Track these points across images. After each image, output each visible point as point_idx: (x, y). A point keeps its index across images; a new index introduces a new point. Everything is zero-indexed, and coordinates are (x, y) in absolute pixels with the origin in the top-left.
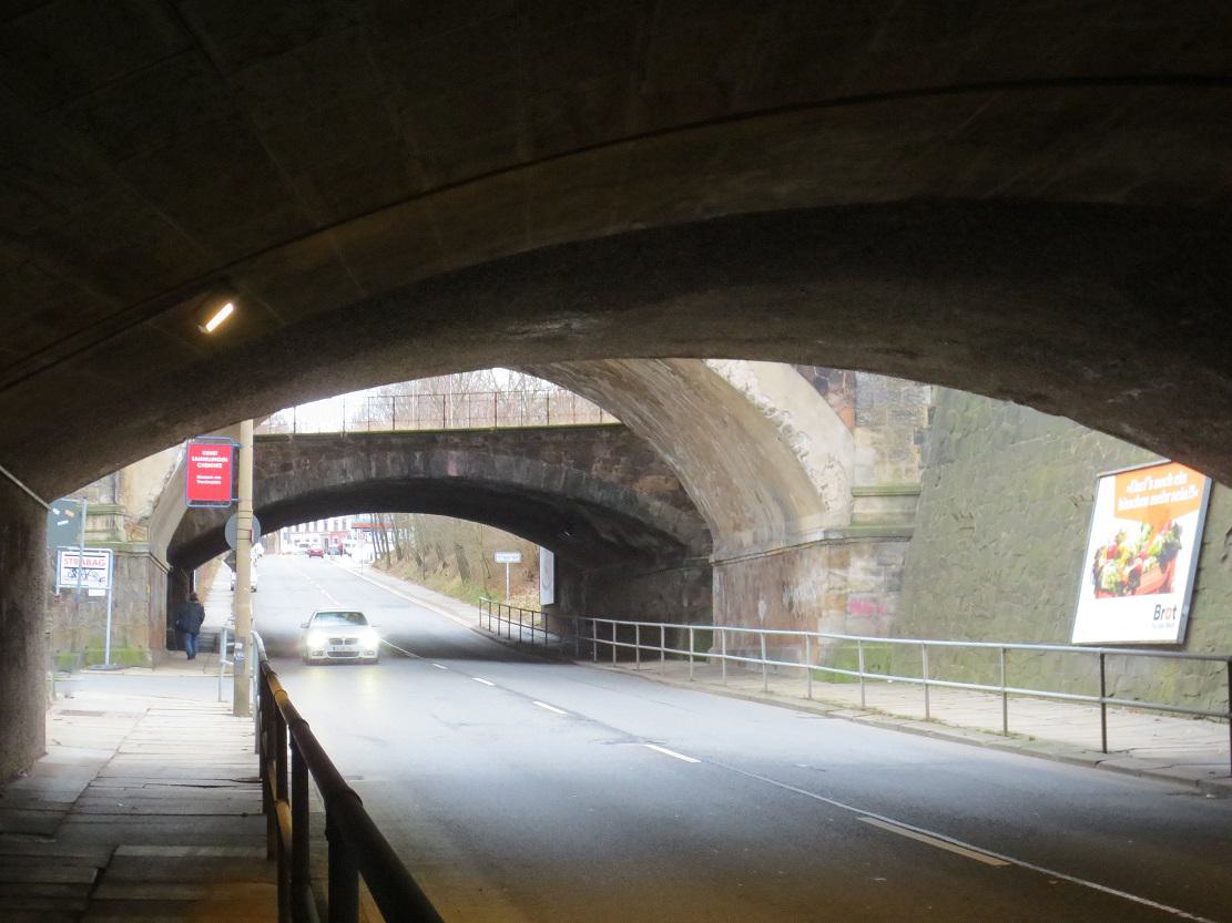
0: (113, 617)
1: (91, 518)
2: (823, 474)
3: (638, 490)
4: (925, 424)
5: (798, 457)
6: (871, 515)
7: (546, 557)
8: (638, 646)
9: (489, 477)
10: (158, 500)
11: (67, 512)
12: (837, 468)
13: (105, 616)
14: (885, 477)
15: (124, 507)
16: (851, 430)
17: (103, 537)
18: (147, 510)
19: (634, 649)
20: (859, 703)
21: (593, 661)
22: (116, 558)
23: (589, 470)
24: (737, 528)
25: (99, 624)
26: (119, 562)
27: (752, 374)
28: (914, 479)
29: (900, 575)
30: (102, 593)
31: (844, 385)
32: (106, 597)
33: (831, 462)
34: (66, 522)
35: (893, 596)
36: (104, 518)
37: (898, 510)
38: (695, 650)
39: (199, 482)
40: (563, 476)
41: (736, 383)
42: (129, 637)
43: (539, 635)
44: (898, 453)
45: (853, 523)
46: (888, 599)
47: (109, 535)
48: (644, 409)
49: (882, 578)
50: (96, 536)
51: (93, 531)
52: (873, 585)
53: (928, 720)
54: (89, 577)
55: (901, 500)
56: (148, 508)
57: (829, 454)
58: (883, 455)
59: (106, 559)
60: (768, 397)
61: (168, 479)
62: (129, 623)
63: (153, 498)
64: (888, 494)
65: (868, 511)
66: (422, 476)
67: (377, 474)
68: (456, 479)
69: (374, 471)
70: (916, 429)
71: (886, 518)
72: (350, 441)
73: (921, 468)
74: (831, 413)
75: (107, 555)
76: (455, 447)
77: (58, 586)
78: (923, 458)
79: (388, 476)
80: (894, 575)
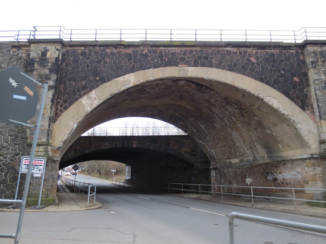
0: (44, 185)
1: (38, 146)
3: (181, 151)
5: (298, 131)
8: (200, 191)
9: (144, 148)
10: (65, 141)
11: (26, 89)
12: (312, 134)
13: (40, 185)
15: (52, 143)
18: (61, 145)
19: (182, 190)
21: (168, 193)
22: (47, 162)
25: (37, 188)
26: (48, 163)
27: (280, 104)
30: (40, 175)
32: (41, 177)
33: (310, 132)
34: (24, 98)
38: (253, 195)
40: (163, 148)
41: (275, 106)
42: (49, 193)
47: (45, 153)
50: (39, 153)
51: (38, 152)
54: (35, 169)
56: (61, 144)
57: (309, 129)
59: (43, 162)
60: (286, 111)
61: (70, 133)
62: (49, 187)
63: (63, 140)
66: (126, 147)
68: (134, 148)
72: (108, 138)
74: (307, 116)
75: (44, 160)
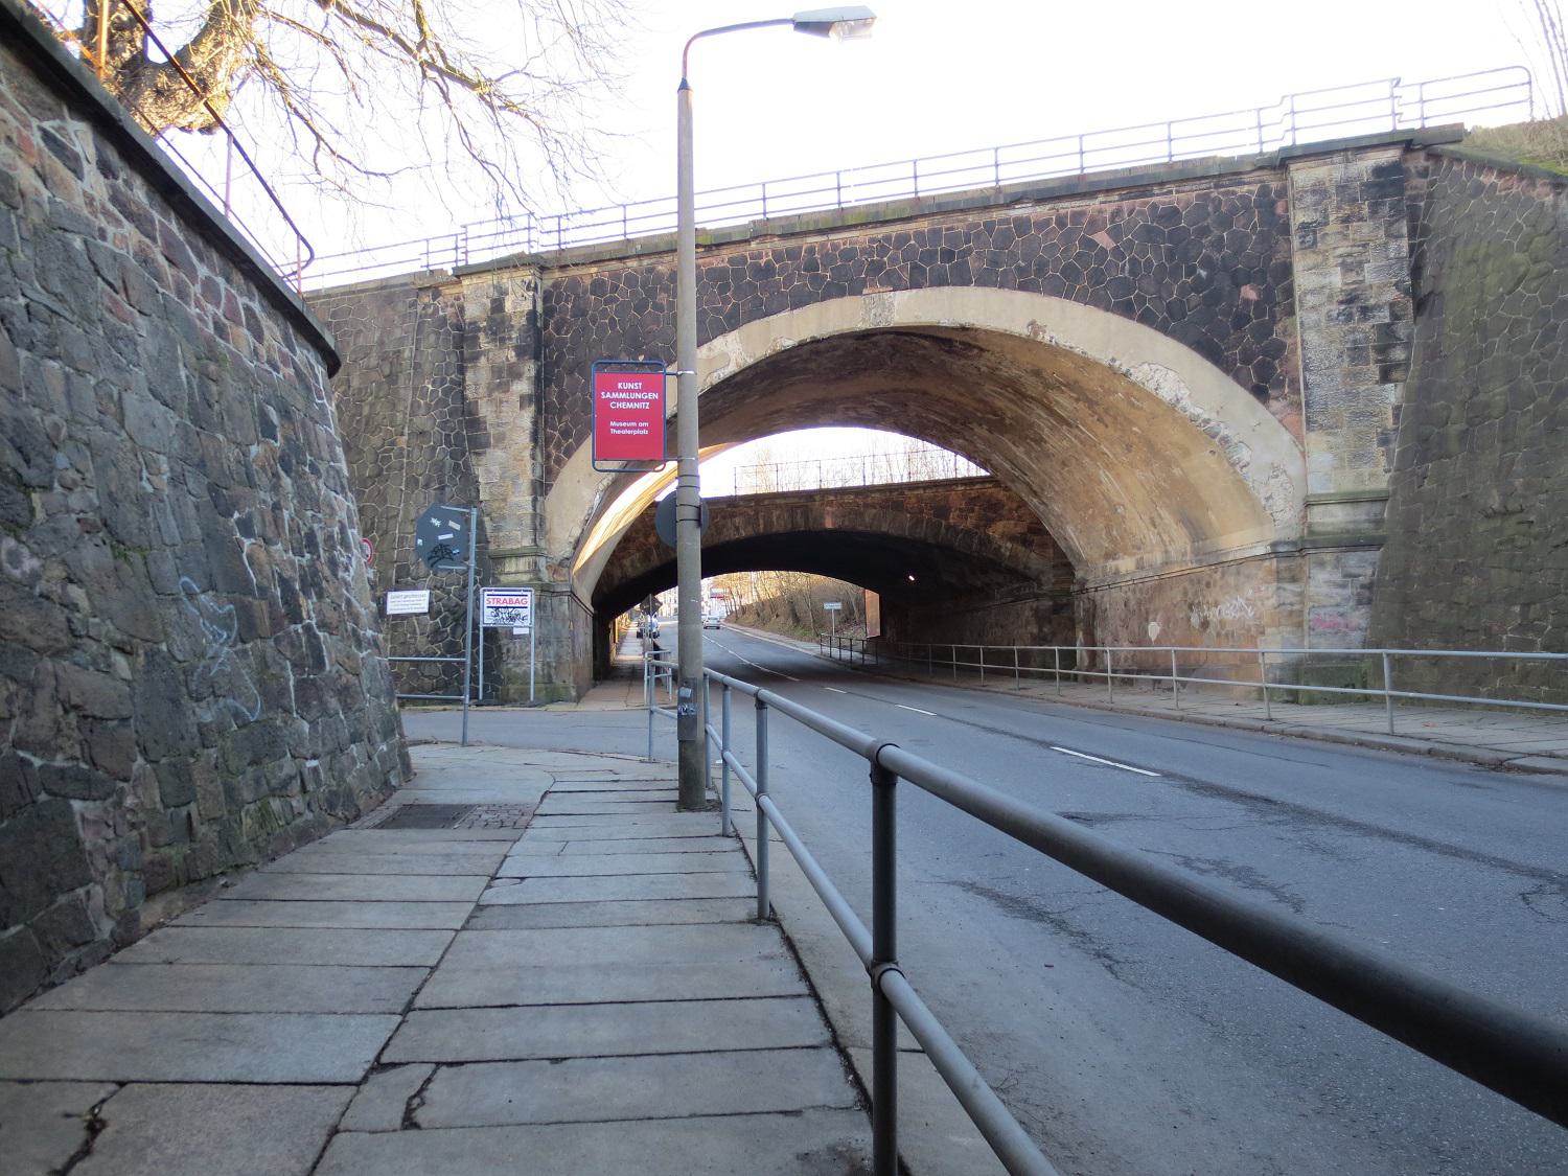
2: (1266, 484)
4: (1390, 424)
5: (1238, 468)
6: (1332, 524)
7: (872, 598)
11: (452, 524)
12: (1282, 478)
14: (1348, 483)
16: (1299, 439)
17: (525, 578)
20: (1387, 729)
23: (947, 519)
24: (1110, 555)
27: (1182, 385)
28: (1382, 483)
29: (1369, 587)
30: (526, 631)
31: (1286, 390)
34: (450, 536)
35: (1363, 610)
36: (527, 559)
37: (1364, 517)
39: (613, 431)
43: (869, 659)
44: (1358, 457)
45: (1311, 532)
46: (1357, 613)
48: (1019, 452)
49: (1348, 591)
51: (516, 573)
52: (1339, 599)
53: (1392, 734)
55: (1366, 507)
58: (1342, 459)
59: (528, 598)
63: (572, 540)
64: (1352, 500)
65: (1328, 520)
67: (765, 527)
68: (831, 532)
69: (762, 526)
70: (1379, 430)
71: (1351, 526)
73: (1386, 471)
76: (830, 503)
77: (481, 626)
78: (1390, 461)
79: (774, 530)
80: (1363, 586)
